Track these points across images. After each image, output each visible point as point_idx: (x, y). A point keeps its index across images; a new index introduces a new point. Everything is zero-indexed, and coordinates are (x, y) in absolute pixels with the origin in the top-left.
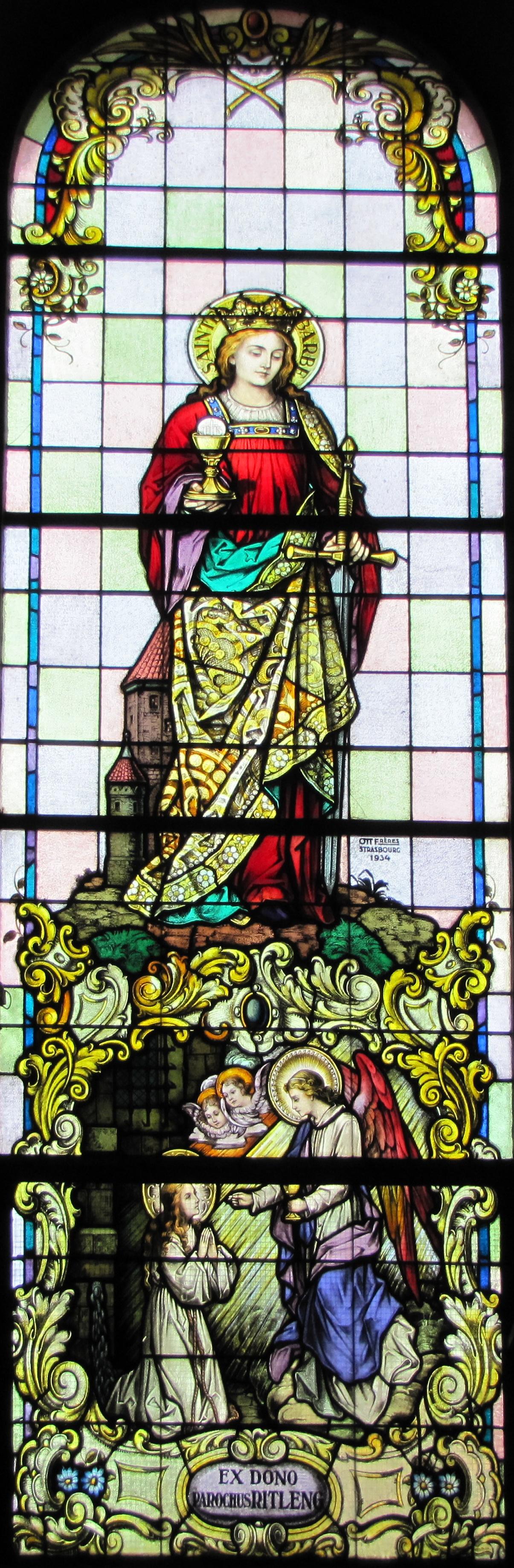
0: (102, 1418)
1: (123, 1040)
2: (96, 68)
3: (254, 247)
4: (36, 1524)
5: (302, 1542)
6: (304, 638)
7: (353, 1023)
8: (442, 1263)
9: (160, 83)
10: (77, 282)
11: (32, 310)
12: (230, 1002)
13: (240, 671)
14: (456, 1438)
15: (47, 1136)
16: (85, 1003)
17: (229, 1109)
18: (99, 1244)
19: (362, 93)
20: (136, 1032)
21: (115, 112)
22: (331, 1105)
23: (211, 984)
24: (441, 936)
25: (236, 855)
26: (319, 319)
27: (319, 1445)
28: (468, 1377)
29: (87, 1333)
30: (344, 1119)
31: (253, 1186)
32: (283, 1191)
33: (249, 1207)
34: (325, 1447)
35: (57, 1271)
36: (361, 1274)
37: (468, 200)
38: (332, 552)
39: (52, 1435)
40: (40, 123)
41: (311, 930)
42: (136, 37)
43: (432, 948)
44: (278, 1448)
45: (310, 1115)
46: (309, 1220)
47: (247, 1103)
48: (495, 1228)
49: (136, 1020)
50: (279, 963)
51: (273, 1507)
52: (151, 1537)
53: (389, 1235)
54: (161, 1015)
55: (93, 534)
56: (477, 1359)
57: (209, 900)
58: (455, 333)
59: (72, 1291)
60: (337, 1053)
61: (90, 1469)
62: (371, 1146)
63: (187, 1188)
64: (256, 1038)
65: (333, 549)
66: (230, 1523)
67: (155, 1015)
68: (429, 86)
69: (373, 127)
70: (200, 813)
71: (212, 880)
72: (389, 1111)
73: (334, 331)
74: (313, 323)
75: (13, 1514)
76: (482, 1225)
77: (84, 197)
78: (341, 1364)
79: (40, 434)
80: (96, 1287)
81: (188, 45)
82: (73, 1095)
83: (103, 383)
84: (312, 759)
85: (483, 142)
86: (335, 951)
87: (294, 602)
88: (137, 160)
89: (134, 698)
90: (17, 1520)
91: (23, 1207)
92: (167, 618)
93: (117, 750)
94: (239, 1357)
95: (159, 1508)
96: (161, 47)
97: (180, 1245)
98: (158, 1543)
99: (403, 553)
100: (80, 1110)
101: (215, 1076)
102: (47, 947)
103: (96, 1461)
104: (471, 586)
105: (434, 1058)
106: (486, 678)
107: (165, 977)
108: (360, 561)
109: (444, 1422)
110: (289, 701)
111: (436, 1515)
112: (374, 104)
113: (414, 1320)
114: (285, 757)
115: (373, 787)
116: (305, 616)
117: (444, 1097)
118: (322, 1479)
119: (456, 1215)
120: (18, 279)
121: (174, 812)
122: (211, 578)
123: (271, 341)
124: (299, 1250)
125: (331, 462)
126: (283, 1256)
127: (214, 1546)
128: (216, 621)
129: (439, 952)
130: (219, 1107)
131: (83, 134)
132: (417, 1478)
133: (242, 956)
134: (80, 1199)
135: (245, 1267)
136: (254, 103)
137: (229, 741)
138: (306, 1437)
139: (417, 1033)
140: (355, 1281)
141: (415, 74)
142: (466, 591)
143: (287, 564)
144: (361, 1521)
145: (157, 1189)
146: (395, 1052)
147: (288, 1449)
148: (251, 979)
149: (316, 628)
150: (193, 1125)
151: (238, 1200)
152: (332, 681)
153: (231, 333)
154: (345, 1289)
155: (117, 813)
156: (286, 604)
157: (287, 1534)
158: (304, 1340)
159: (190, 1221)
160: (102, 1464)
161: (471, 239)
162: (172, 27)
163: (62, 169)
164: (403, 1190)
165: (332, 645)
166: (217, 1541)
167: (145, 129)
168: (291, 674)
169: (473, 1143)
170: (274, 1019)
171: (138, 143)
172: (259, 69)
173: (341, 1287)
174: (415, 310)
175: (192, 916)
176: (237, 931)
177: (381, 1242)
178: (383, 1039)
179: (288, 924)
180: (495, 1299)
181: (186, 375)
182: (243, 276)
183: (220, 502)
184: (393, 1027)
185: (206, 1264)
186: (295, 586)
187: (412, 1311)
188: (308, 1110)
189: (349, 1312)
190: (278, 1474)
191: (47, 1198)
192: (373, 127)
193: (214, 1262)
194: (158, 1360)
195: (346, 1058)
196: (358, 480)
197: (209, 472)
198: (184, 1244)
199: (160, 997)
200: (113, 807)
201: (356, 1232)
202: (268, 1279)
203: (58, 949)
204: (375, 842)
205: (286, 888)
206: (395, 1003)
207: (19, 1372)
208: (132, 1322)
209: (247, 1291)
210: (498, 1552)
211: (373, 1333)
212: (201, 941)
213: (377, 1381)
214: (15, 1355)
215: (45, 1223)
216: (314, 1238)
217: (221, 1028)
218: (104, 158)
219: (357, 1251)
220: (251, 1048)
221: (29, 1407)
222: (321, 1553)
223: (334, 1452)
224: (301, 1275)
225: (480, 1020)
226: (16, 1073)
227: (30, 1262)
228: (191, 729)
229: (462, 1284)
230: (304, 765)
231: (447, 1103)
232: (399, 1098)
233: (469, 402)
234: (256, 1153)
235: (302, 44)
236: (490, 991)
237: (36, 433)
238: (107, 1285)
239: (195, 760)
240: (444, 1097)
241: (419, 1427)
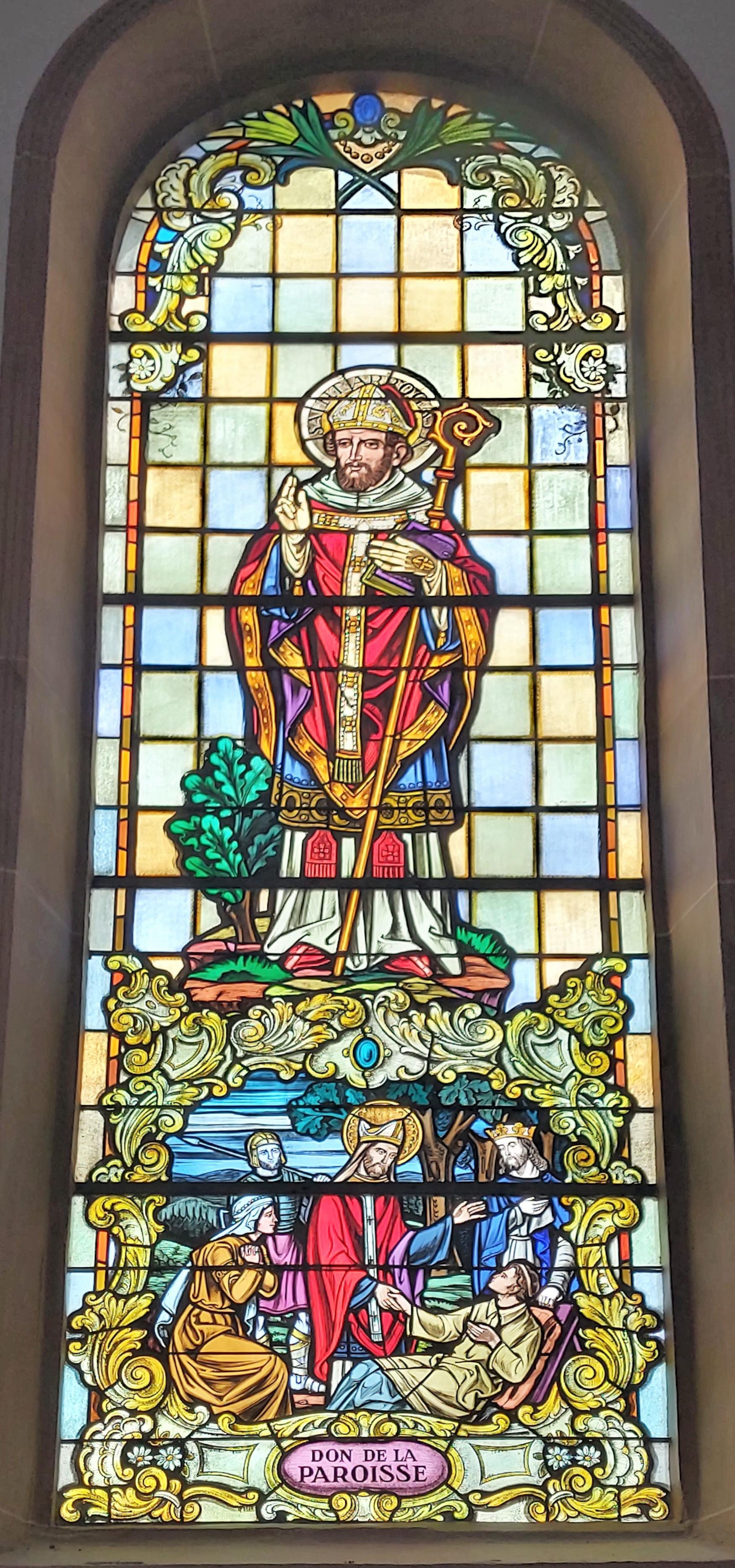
15: (129, 1163)
67: (257, 1054)
88: (250, 248)
120: (119, 367)
146: (522, 1087)
157: (304, 1063)
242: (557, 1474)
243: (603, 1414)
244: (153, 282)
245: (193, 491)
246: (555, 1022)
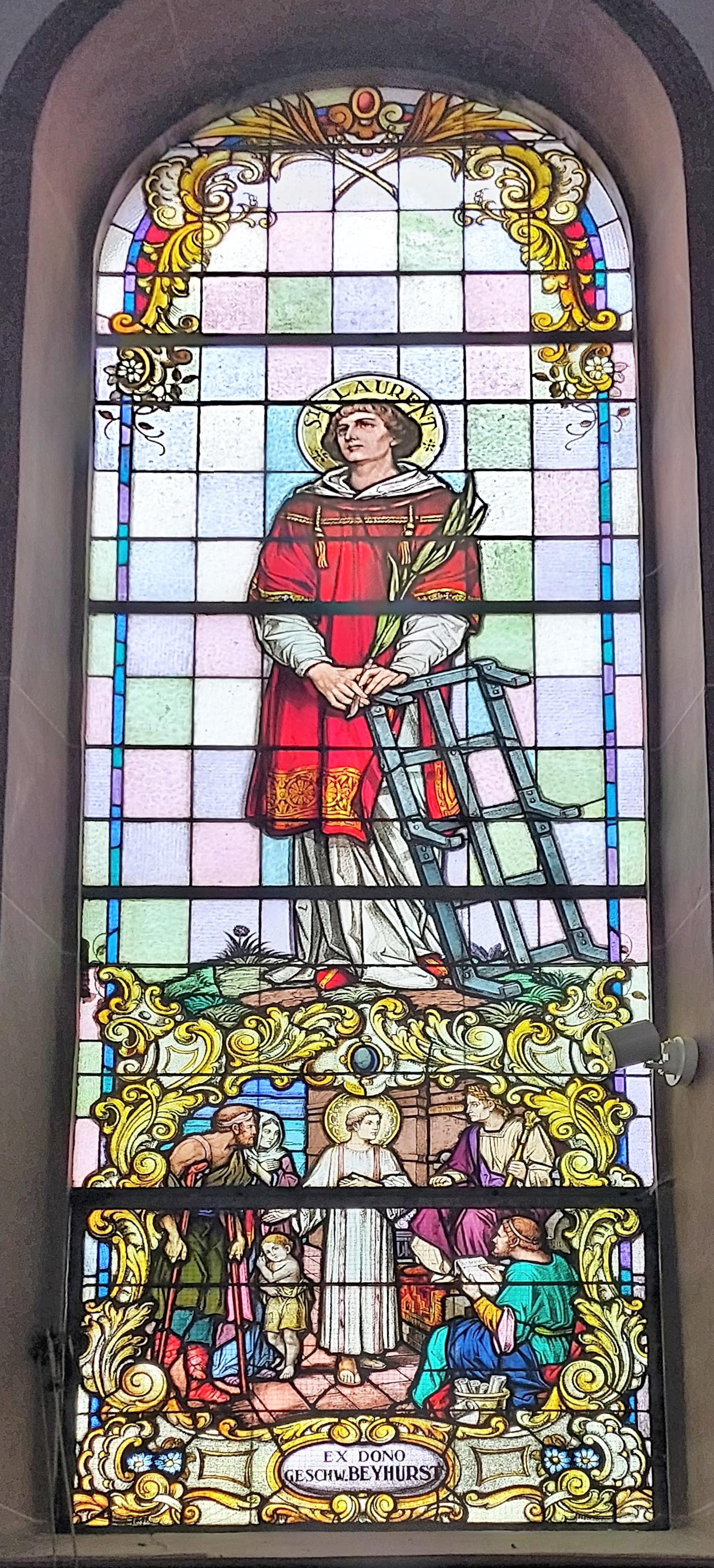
2: (194, 153)
15: (124, 1169)
20: (229, 1079)
21: (213, 199)
26: (438, 403)
40: (130, 211)
54: (259, 1063)
67: (253, 1063)
88: (238, 247)
119: (592, 1233)
127: (311, 1515)
131: (179, 221)
133: (350, 1012)
141: (539, 147)
146: (522, 1094)
163: (154, 257)
169: (611, 1171)
171: (239, 230)
172: (374, 148)
192: (497, 206)
203: (143, 1007)
215: (122, 1246)
221: (95, 1402)
237: (125, 523)
243: (602, 1417)
244: (143, 283)
245: (187, 498)
246: (557, 1030)
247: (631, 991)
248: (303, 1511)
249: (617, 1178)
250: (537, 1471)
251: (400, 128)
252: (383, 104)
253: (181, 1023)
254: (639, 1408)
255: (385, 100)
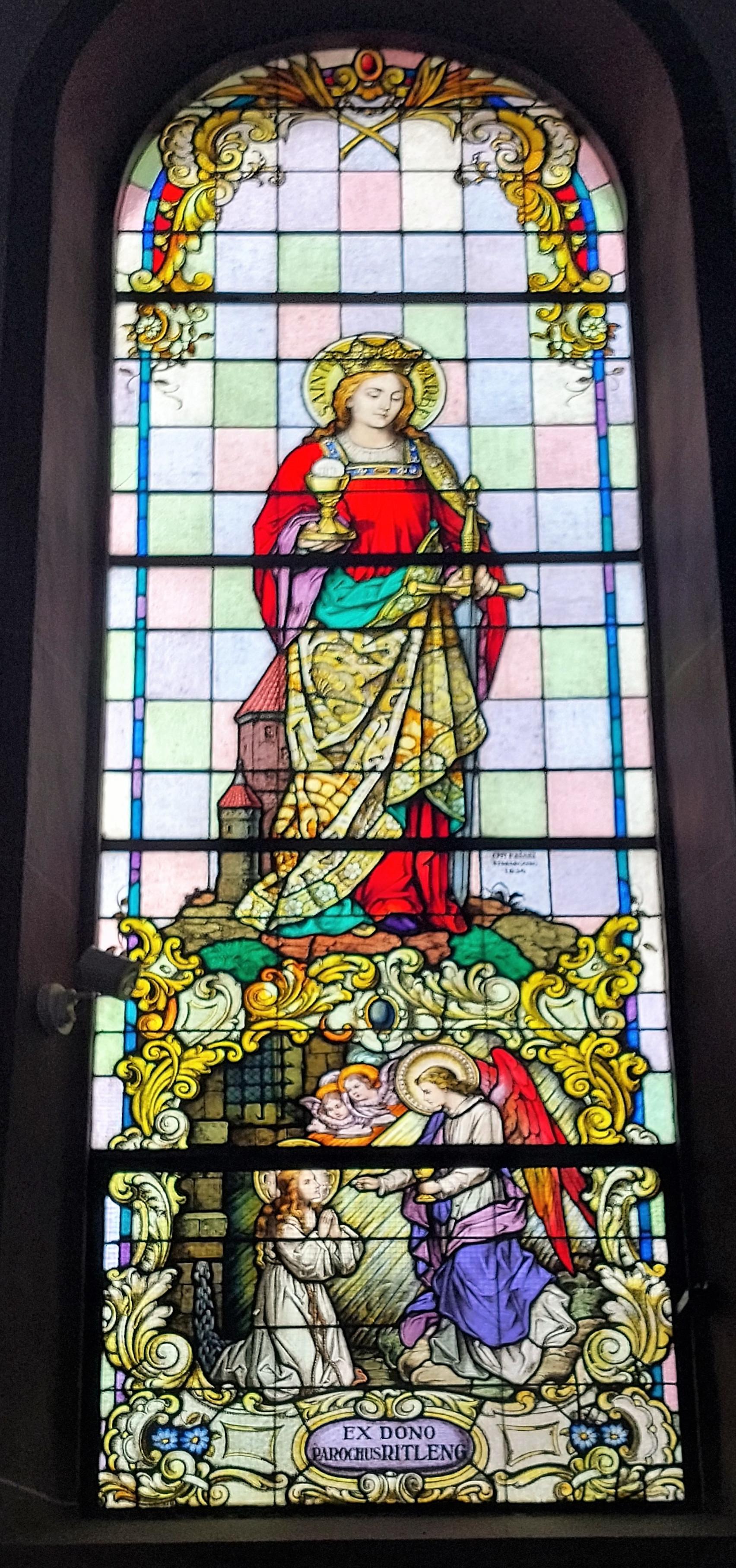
0: (206, 1384)
1: (235, 1041)
2: (206, 113)
3: (370, 290)
4: (128, 1480)
5: (442, 1490)
6: (429, 669)
7: (490, 1022)
8: (598, 1237)
9: (273, 127)
10: (186, 328)
11: (138, 355)
12: (353, 1005)
13: (361, 701)
14: (620, 1394)
15: (147, 1131)
16: (192, 1010)
17: (352, 1102)
18: (206, 1227)
19: (479, 133)
20: (249, 1034)
21: (225, 157)
22: (467, 1096)
23: (332, 989)
24: (582, 943)
25: (359, 872)
26: (440, 361)
27: (460, 1404)
28: (632, 1340)
29: (191, 1307)
30: (482, 1109)
31: (380, 1171)
32: (414, 1175)
33: (376, 1191)
34: (467, 1405)
35: (157, 1254)
36: (506, 1249)
37: (592, 238)
38: (458, 587)
39: (147, 1401)
40: (146, 168)
41: (442, 937)
42: (247, 81)
43: (574, 952)
44: (413, 1407)
45: (443, 1106)
46: (445, 1200)
47: (374, 1097)
48: (657, 1207)
49: (248, 1025)
50: (406, 968)
51: (407, 1459)
52: (263, 1488)
53: (536, 1212)
55: (204, 573)
56: (643, 1323)
57: (329, 913)
58: (583, 370)
59: (174, 1271)
60: (473, 1049)
61: (192, 1430)
62: (512, 1133)
63: (306, 1174)
64: (383, 1037)
65: (458, 582)
66: (356, 1474)
68: (548, 125)
69: (492, 167)
70: (318, 834)
71: (333, 894)
72: (531, 1102)
73: (456, 371)
74: (434, 364)
75: (99, 1471)
76: (642, 1202)
77: (194, 242)
78: (485, 1330)
79: (146, 478)
80: (202, 1266)
81: (298, 86)
82: (178, 1093)
83: (213, 427)
84: (440, 781)
85: (606, 179)
86: (468, 957)
87: (417, 635)
88: (249, 205)
89: (248, 729)
90: (103, 1477)
91: (120, 1196)
92: (282, 652)
93: (230, 777)
94: (367, 1326)
95: (274, 1463)
96: (273, 90)
97: (298, 1226)
98: (271, 1493)
99: (533, 586)
100: (185, 1106)
101: (337, 1073)
102: (151, 959)
103: (198, 1422)
104: (607, 615)
105: (580, 1053)
106: (624, 703)
107: (280, 984)
108: (486, 596)
109: (606, 1380)
110: (414, 728)
111: (600, 1462)
112: (494, 149)
113: (567, 1288)
114: (411, 780)
115: (504, 806)
116: (428, 648)
117: (592, 1088)
118: (465, 1433)
119: (610, 1194)
121: (291, 834)
122: (331, 614)
123: (389, 382)
124: (432, 1228)
125: (455, 501)
126: (415, 1235)
127: (337, 1494)
128: (336, 655)
129: (583, 956)
130: (342, 1100)
132: (575, 1429)
133: (365, 963)
134: (184, 1187)
135: (371, 1245)
136: (368, 143)
137: (349, 766)
138: (443, 1395)
139: (561, 1030)
140: (499, 1254)
141: (534, 113)
142: (601, 620)
143: (410, 599)
144: (510, 1470)
145: (272, 1175)
147: (424, 1406)
148: (377, 982)
149: (442, 659)
150: (312, 1117)
151: (363, 1184)
152: (459, 709)
153: (347, 376)
154: (487, 1263)
155: (229, 836)
156: (409, 637)
157: (424, 1482)
158: (441, 1310)
159: (309, 1204)
160: (205, 1424)
161: (596, 277)
162: (283, 70)
164: (550, 1172)
165: (459, 675)
166: (341, 1491)
167: (256, 174)
168: (416, 703)
170: (401, 1019)
171: (249, 186)
173: (482, 1261)
174: (540, 348)
175: (310, 928)
176: (361, 940)
177: (527, 1219)
178: (522, 1036)
179: (417, 933)
180: (660, 1270)
181: (302, 416)
182: (358, 319)
183: (338, 541)
184: (533, 1025)
185: (328, 1243)
186: (419, 620)
187: (564, 1281)
188: (442, 1102)
189: (494, 1282)
190: (412, 1430)
191: (147, 1187)
192: (492, 167)
193: (337, 1240)
194: (272, 1331)
195: (482, 1054)
196: (483, 518)
197: (326, 512)
198: (302, 1226)
199: (276, 1002)
200: (225, 829)
201: (498, 1211)
202: (398, 1255)
203: (164, 960)
204: (507, 856)
205: (414, 901)
206: (535, 1002)
207: (111, 1344)
208: (242, 1297)
209: (375, 1266)
210: (675, 1493)
211: (521, 1302)
212: (320, 950)
213: (526, 1344)
214: (105, 1330)
215: (144, 1211)
216: (450, 1218)
217: (343, 1030)
218: (213, 202)
219: (499, 1228)
220: (377, 1047)
222: (465, 1499)
223: (479, 1410)
224: (437, 1249)
225: (631, 1018)
226: (115, 1074)
227: (126, 1246)
228: (308, 756)
229: (622, 1256)
230: (431, 786)
231: (595, 1093)
232: (542, 1089)
233: (600, 438)
234: (383, 1141)
235: (416, 85)
236: (641, 990)
237: (143, 475)
238: (214, 1265)
239: (313, 785)
240: (592, 1088)
241: (577, 1385)
242: (582, 1453)
247: (643, 942)
248: (330, 1492)
249: (636, 1137)
250: (568, 1450)
251: (402, 91)
252: (385, 68)
253: (201, 977)
254: (665, 1381)
255: (388, 63)
